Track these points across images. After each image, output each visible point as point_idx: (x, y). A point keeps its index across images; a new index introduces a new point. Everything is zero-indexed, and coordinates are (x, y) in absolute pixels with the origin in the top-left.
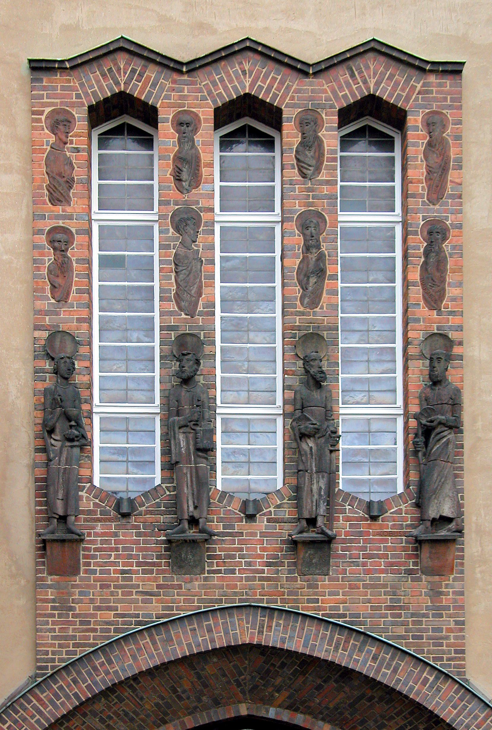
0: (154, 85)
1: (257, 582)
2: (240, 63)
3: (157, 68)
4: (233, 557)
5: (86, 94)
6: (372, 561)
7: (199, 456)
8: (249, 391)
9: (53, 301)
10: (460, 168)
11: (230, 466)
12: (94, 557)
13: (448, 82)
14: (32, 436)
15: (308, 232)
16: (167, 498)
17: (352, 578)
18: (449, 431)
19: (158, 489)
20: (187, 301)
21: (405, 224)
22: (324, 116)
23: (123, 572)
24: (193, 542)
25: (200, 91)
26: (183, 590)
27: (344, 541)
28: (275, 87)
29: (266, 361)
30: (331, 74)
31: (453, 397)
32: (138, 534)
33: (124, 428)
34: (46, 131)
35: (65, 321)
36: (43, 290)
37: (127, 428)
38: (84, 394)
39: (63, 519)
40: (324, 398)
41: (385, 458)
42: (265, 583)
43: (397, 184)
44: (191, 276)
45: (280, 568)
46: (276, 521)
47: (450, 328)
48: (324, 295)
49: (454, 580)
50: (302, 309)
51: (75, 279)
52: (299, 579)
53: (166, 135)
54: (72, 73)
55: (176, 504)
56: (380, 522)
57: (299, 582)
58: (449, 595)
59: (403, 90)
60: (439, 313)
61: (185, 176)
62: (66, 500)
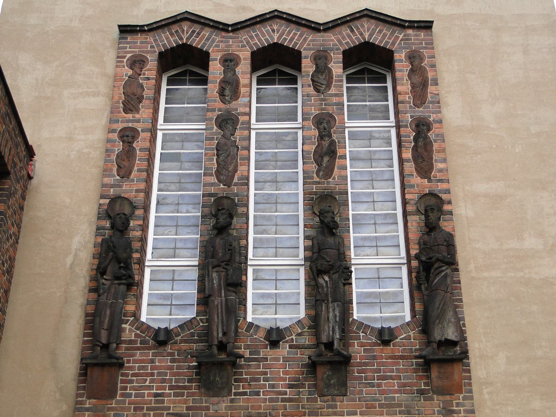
0: (208, 39)
1: (280, 403)
2: (271, 26)
3: (210, 30)
4: (258, 380)
5: (158, 46)
6: (386, 383)
7: (229, 290)
8: (276, 248)
9: (118, 178)
10: (437, 84)
11: (259, 307)
12: (131, 382)
13: (422, 34)
14: (88, 279)
15: (322, 127)
16: (201, 329)
17: (368, 398)
18: (446, 267)
19: (193, 320)
20: (225, 175)
21: (398, 127)
22: (332, 55)
23: (156, 395)
24: (221, 364)
25: (241, 42)
26: (211, 411)
27: (360, 364)
28: (296, 38)
29: (291, 225)
30: (337, 29)
31: (447, 239)
32: (173, 361)
33: (171, 278)
34: (126, 68)
35: (126, 192)
36: (111, 170)
37: (173, 278)
38: (136, 245)
39: (106, 347)
40: (337, 243)
41: (393, 300)
42: (288, 404)
43: (391, 103)
44: (229, 158)
45: (301, 390)
46: (297, 347)
47: (440, 191)
48: (336, 169)
49: (464, 398)
50: (318, 180)
51: (137, 162)
52: (319, 399)
53: (216, 70)
54: (149, 34)
55: (207, 333)
56: (392, 347)
57: (319, 403)
58: (461, 413)
59: (389, 38)
60: (430, 180)
61: (227, 92)
62: (110, 329)
